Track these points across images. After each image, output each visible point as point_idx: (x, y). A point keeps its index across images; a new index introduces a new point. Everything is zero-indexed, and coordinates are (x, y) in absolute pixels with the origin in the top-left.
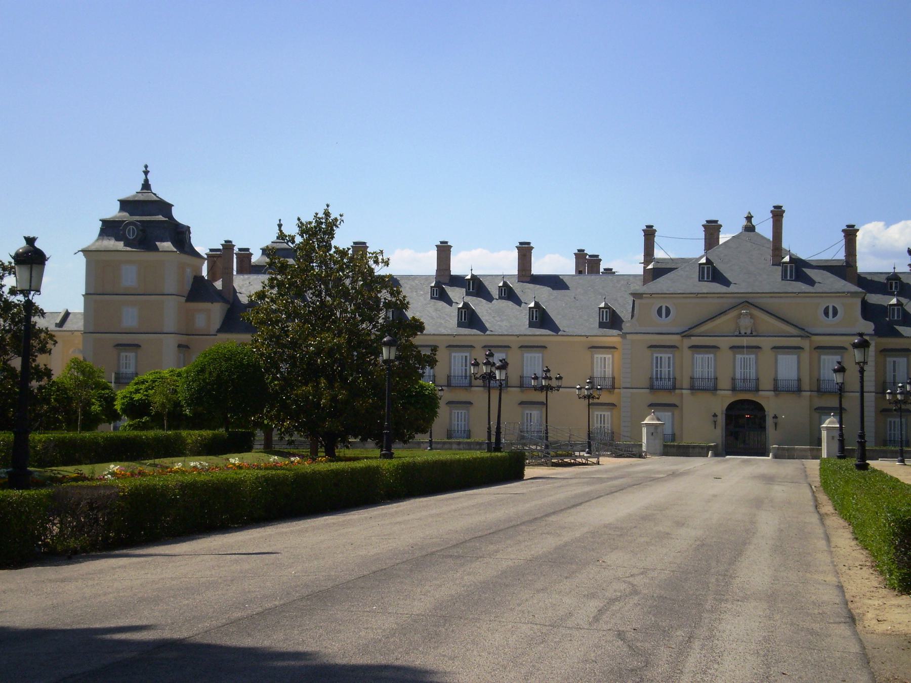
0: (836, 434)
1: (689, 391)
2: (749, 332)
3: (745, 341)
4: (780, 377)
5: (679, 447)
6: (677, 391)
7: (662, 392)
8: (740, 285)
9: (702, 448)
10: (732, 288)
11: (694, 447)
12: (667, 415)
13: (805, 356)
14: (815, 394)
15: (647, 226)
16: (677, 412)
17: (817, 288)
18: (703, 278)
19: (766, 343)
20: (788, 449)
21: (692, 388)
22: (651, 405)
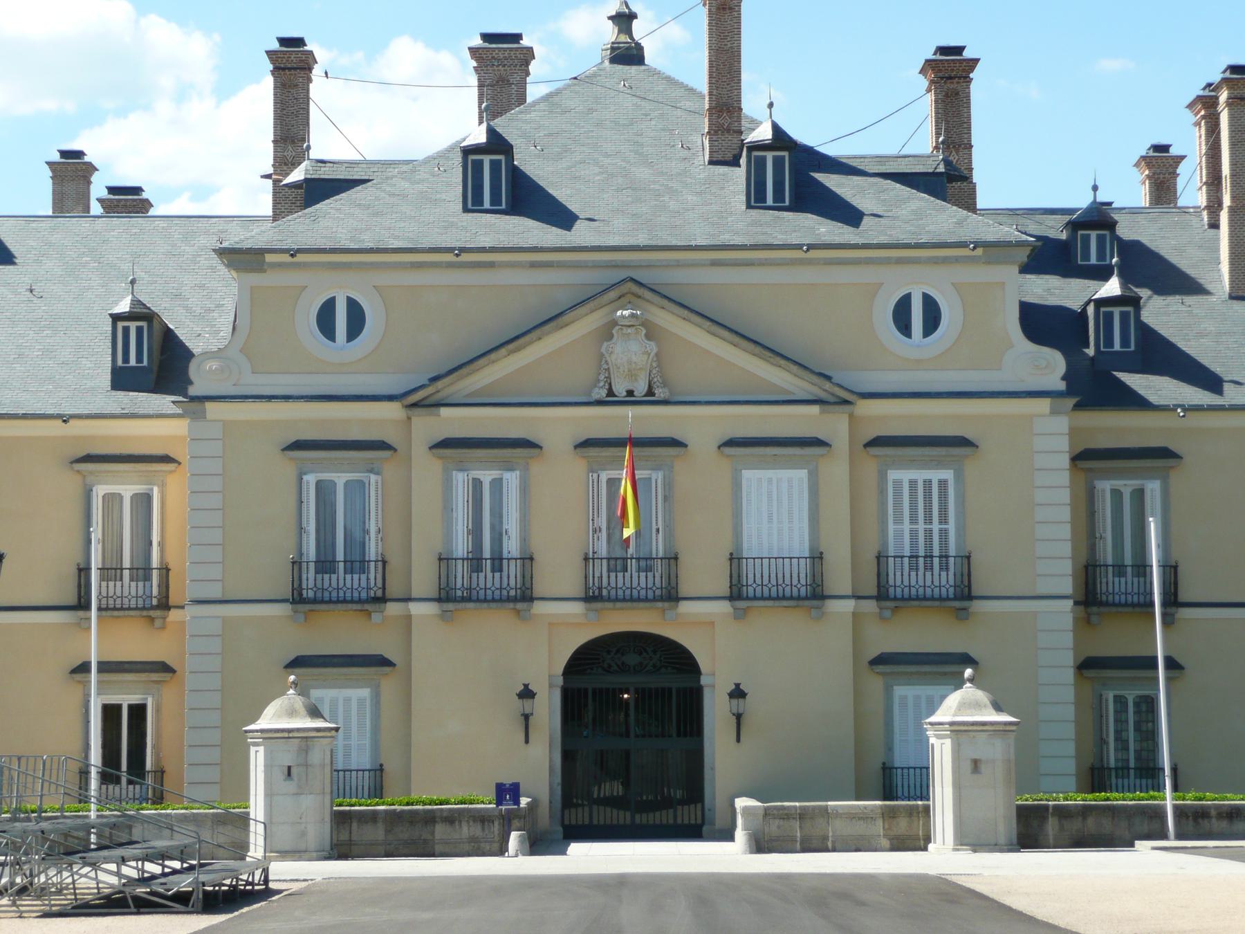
0: (996, 752)
1: (430, 609)
2: (641, 388)
3: (629, 420)
4: (751, 547)
5: (394, 819)
6: (392, 609)
7: (335, 597)
8: (609, 218)
9: (482, 819)
10: (581, 234)
11: (451, 819)
12: (349, 698)
13: (836, 469)
14: (870, 606)
15: (284, 41)
16: (389, 683)
17: (869, 231)
18: (478, 199)
19: (702, 426)
20: (803, 815)
21: (445, 596)
22: (298, 663)
